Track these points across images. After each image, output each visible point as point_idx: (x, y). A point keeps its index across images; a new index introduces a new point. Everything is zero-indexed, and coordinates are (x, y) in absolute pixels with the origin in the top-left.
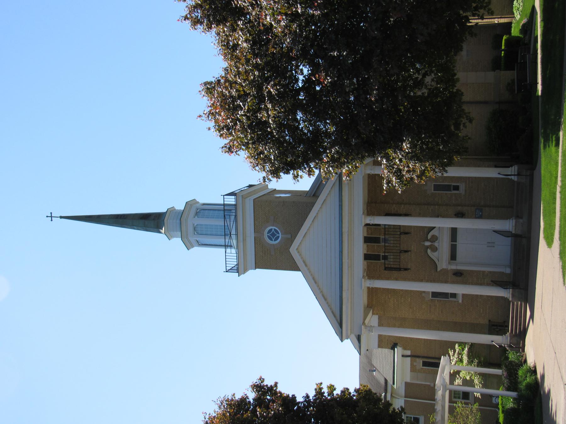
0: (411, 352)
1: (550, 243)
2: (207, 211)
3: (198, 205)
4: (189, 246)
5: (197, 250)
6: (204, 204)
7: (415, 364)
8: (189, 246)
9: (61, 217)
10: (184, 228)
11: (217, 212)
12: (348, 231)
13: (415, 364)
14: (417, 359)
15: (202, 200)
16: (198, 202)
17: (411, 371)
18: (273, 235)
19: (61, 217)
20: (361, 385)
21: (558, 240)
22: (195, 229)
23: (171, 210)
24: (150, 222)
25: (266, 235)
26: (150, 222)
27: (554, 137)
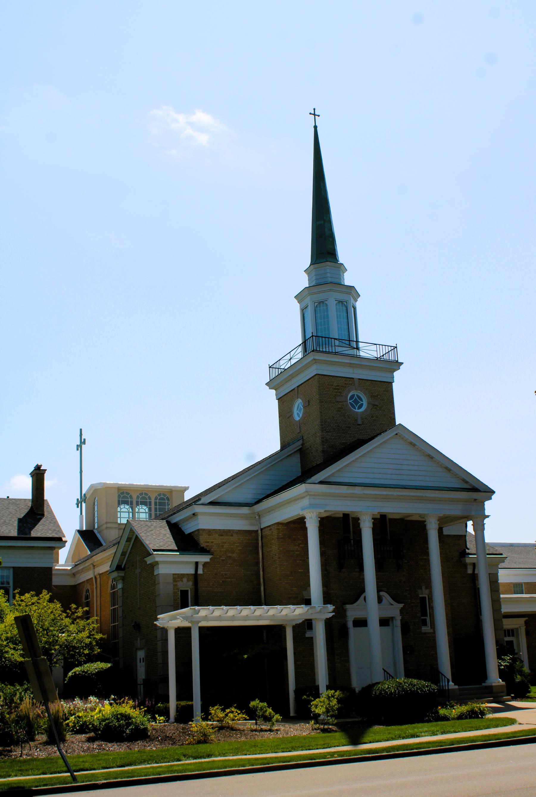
0: (201, 574)
1: (512, 722)
2: (345, 314)
3: (352, 301)
4: (299, 297)
5: (296, 307)
6: (355, 309)
7: (185, 580)
8: (299, 297)
9: (315, 127)
10: (319, 289)
11: (346, 327)
12: (426, 497)
13: (185, 580)
14: (190, 584)
15: (359, 305)
16: (356, 301)
17: (174, 574)
18: (356, 402)
19: (315, 127)
20: (488, 544)
21: (498, 728)
22: (321, 303)
23: (340, 268)
24: (324, 245)
25: (355, 393)
26: (324, 245)
27: (490, 716)
